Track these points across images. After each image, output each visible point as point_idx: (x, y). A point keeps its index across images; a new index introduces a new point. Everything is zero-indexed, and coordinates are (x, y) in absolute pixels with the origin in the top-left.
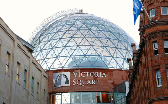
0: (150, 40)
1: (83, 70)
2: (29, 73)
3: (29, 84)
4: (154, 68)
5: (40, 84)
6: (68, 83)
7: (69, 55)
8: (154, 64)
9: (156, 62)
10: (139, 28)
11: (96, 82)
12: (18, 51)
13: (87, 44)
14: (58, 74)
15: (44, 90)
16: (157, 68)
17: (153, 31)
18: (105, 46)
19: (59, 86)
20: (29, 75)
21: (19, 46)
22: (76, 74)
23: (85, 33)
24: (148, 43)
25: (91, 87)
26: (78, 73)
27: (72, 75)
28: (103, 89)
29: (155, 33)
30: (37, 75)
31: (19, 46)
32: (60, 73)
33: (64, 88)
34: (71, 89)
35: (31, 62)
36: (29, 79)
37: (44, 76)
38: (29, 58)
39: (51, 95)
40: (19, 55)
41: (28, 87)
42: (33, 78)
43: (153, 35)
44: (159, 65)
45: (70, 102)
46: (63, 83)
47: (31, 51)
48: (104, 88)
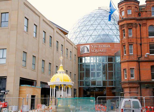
0: (121, 29)
3: (64, 53)
4: (123, 45)
5: (72, 52)
7: (86, 29)
8: (123, 43)
11: (104, 51)
12: (56, 35)
13: (97, 23)
14: (83, 46)
15: (75, 55)
16: (124, 45)
17: (123, 24)
18: (111, 29)
19: (84, 53)
20: (64, 48)
21: (57, 32)
22: (93, 46)
25: (101, 54)
28: (109, 54)
29: (124, 25)
30: (70, 48)
31: (57, 32)
32: (84, 46)
34: (90, 55)
35: (65, 40)
36: (64, 50)
37: (74, 47)
38: (64, 38)
39: (80, 58)
40: (57, 37)
41: (64, 54)
43: (123, 26)
45: (139, 64)
46: (86, 51)
48: (109, 54)
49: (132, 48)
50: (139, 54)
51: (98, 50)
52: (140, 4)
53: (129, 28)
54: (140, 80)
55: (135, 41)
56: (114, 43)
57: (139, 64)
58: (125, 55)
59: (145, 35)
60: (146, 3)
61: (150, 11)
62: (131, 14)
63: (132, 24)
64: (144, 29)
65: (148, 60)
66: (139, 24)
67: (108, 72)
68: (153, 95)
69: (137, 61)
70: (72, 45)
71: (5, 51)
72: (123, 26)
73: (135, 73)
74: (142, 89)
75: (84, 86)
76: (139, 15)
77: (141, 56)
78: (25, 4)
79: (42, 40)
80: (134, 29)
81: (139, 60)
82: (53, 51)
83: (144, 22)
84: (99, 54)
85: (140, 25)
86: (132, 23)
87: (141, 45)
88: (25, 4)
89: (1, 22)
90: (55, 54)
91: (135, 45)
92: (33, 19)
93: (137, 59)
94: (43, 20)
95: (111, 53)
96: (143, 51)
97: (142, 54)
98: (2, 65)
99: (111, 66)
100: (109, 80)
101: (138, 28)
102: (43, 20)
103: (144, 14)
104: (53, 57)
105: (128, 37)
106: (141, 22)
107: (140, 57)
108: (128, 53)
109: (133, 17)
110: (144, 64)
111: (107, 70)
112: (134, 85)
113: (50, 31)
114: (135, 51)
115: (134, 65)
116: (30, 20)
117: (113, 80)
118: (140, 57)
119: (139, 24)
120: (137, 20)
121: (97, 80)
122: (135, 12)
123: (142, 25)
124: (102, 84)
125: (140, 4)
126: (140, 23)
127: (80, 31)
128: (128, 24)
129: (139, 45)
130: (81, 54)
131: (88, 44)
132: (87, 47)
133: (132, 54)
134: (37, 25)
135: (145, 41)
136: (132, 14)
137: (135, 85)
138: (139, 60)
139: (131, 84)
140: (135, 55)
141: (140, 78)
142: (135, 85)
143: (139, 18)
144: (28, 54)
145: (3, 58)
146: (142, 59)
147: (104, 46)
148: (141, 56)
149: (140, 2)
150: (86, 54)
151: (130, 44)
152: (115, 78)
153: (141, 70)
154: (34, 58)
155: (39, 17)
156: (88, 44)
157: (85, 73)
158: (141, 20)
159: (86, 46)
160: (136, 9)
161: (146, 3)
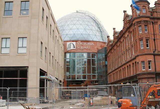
1: (82, 41)
6: (74, 48)
8: (140, 37)
9: (141, 36)
11: (88, 48)
17: (139, 20)
18: (91, 30)
19: (70, 49)
23: (81, 22)
25: (86, 50)
26: (80, 43)
27: (76, 44)
28: (92, 51)
29: (140, 21)
33: (72, 50)
44: (142, 38)
45: (154, 57)
47: (145, 25)
48: (92, 50)
50: (154, 48)
51: (83, 47)
53: (138, 25)
54: (156, 72)
57: (154, 57)
58: (142, 49)
60: (155, 5)
66: (152, 22)
71: (8, 40)
73: (152, 65)
74: (157, 79)
77: (155, 50)
83: (156, 21)
84: (84, 50)
87: (154, 40)
98: (22, 54)
101: (151, 25)
103: (155, 14)
106: (153, 21)
107: (155, 51)
112: (152, 75)
118: (155, 51)
119: (152, 22)
127: (71, 28)
128: (144, 21)
130: (68, 50)
131: (73, 41)
141: (155, 69)
145: (6, 47)
150: (72, 50)
153: (156, 63)
157: (86, 68)
158: (154, 18)
159: (73, 43)
161: (155, 5)
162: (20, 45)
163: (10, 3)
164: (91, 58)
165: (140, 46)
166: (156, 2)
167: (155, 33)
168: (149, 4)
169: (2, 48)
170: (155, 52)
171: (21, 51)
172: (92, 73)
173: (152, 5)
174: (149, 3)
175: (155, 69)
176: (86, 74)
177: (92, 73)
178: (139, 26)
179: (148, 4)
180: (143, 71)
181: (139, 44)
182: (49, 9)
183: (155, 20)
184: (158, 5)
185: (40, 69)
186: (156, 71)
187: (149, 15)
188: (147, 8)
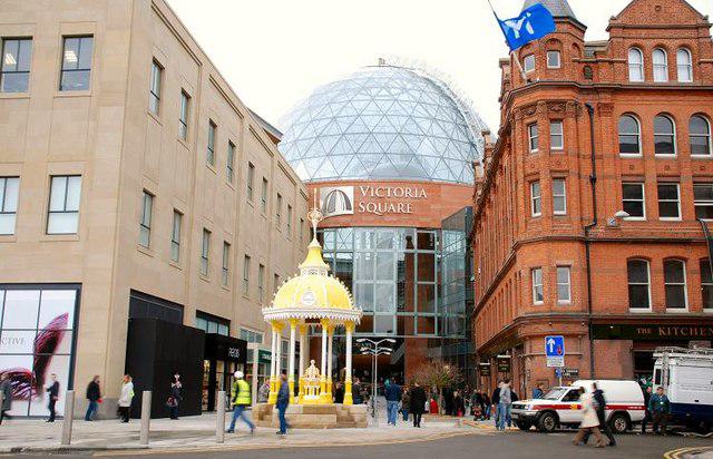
2: (240, 174)
8: (529, 171)
10: (500, 96)
12: (249, 139)
14: (330, 189)
16: (535, 177)
17: (531, 101)
19: (331, 214)
21: (251, 129)
24: (518, 126)
25: (395, 219)
26: (370, 189)
27: (356, 193)
29: (534, 105)
31: (251, 129)
37: (302, 192)
38: (272, 155)
40: (250, 149)
42: (279, 196)
47: (276, 141)
48: (421, 219)
49: (562, 192)
50: (588, 213)
51: (383, 205)
52: (589, 37)
53: (528, 121)
54: (590, 311)
55: (574, 170)
56: (439, 185)
59: (606, 147)
61: (624, 62)
62: (559, 66)
63: (562, 103)
64: (603, 123)
65: (617, 236)
66: (587, 106)
67: (416, 286)
68: (619, 369)
69: (581, 241)
70: (295, 184)
72: (530, 110)
75: (642, 215)
76: (587, 73)
77: (595, 220)
78: (155, 8)
79: (203, 153)
80: (571, 121)
81: (587, 235)
82: (239, 197)
83: (605, 98)
85: (591, 112)
86: (564, 102)
87: (593, 180)
88: (155, 8)
89: (62, 71)
90: (242, 212)
91: (573, 180)
92: (180, 71)
93: (581, 235)
94: (212, 80)
95: (429, 220)
96: (600, 205)
97: (598, 216)
98: (61, 238)
99: (428, 265)
100: (420, 314)
101: (584, 118)
102: (212, 80)
104: (237, 221)
105: (550, 153)
106: (592, 100)
108: (549, 210)
109: (567, 78)
110: (602, 250)
111: (412, 276)
113: (229, 127)
114: (575, 204)
115: (571, 255)
116: (168, 71)
117: (435, 314)
119: (587, 106)
120: (581, 90)
121: (377, 313)
122: (574, 61)
123: (596, 112)
124: (395, 328)
125: (589, 37)
126: (589, 102)
128: (550, 103)
129: (586, 182)
131: (348, 183)
132: (345, 196)
133: (564, 213)
134: (190, 93)
135: (606, 169)
136: (562, 68)
137: (572, 329)
138: (587, 235)
139: (559, 322)
140: (575, 218)
141: (590, 302)
142: (572, 329)
143: (586, 83)
144: (157, 200)
146: (599, 232)
147: (406, 191)
148: (595, 220)
149: (587, 31)
151: (558, 177)
152: (441, 308)
154: (178, 217)
155: (199, 64)
156: (348, 183)
158: (596, 90)
160: (576, 52)
161: (606, 36)
162: (57, 205)
163: (82, 40)
164: (416, 251)
165: (527, 204)
166: (613, 19)
167: (598, 153)
168: (582, 28)
169: (49, 212)
170: (590, 231)
171: (60, 225)
172: (418, 311)
173: (596, 33)
174: (582, 25)
175: (590, 302)
176: (433, 314)
177: (418, 311)
178: (528, 125)
179: (574, 31)
180: (536, 306)
181: (527, 197)
182: (199, 64)
183: (602, 95)
184: (620, 32)
185: (132, 290)
186: (593, 309)
187: (570, 76)
188: (568, 47)
